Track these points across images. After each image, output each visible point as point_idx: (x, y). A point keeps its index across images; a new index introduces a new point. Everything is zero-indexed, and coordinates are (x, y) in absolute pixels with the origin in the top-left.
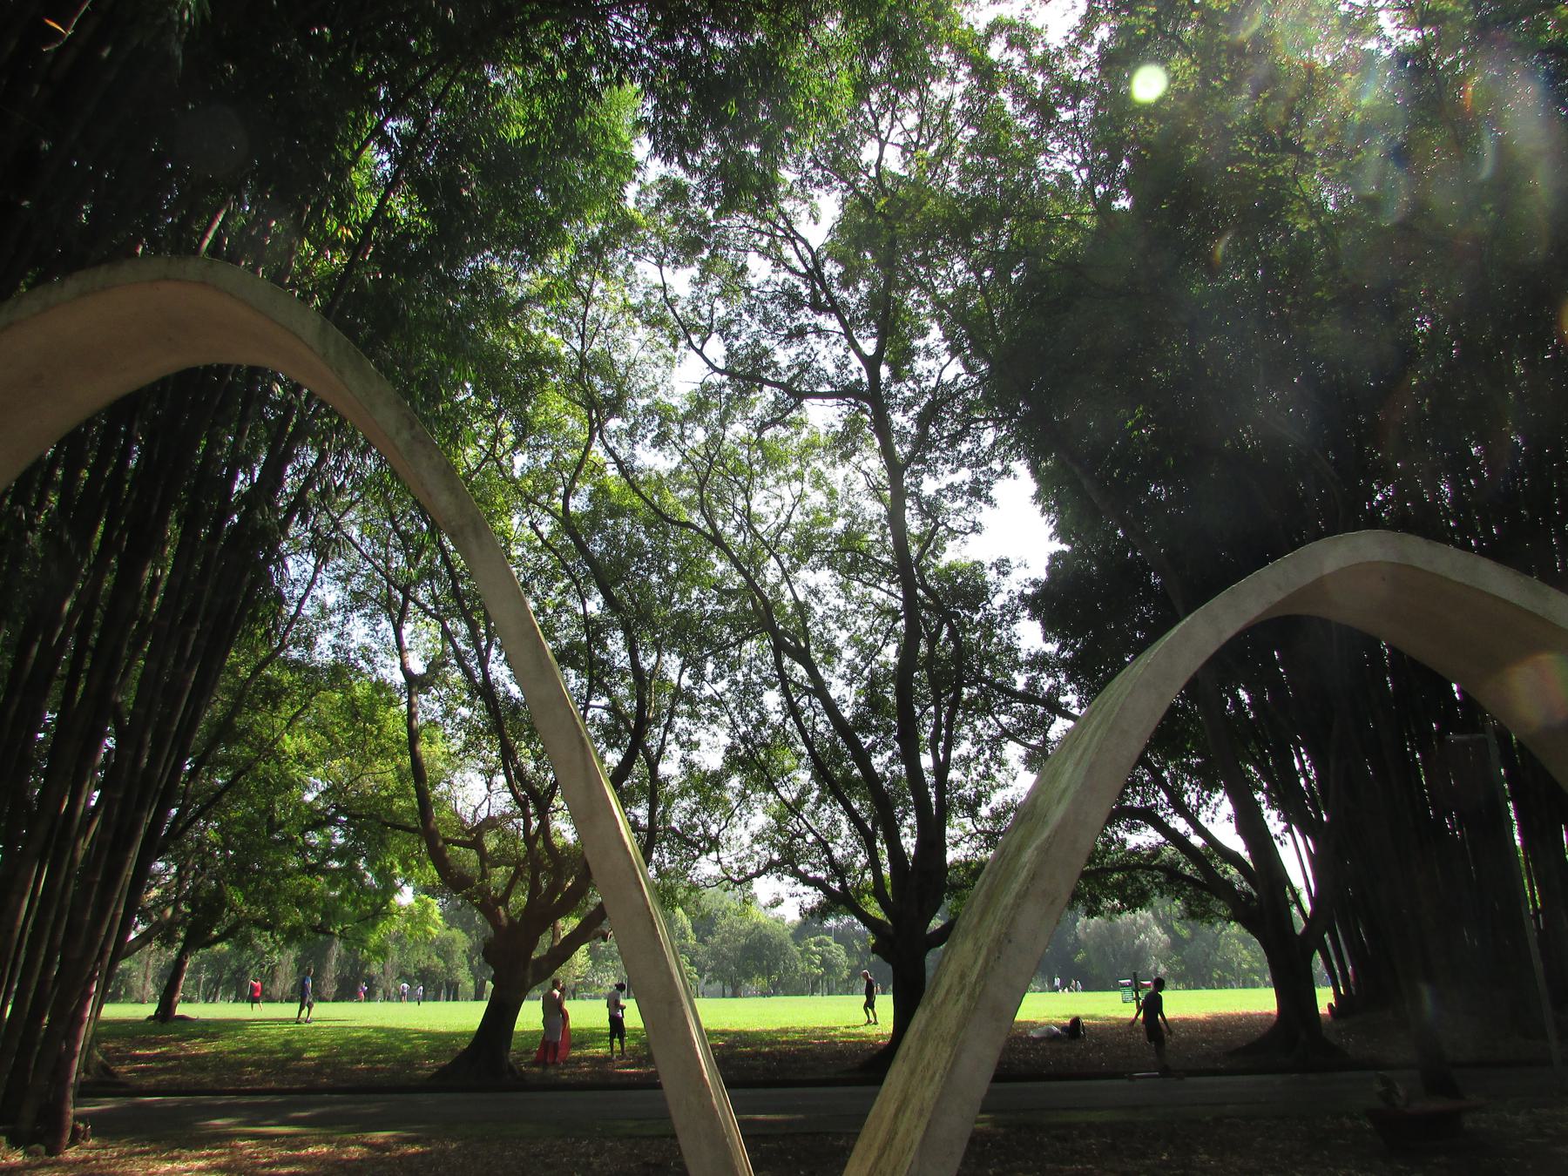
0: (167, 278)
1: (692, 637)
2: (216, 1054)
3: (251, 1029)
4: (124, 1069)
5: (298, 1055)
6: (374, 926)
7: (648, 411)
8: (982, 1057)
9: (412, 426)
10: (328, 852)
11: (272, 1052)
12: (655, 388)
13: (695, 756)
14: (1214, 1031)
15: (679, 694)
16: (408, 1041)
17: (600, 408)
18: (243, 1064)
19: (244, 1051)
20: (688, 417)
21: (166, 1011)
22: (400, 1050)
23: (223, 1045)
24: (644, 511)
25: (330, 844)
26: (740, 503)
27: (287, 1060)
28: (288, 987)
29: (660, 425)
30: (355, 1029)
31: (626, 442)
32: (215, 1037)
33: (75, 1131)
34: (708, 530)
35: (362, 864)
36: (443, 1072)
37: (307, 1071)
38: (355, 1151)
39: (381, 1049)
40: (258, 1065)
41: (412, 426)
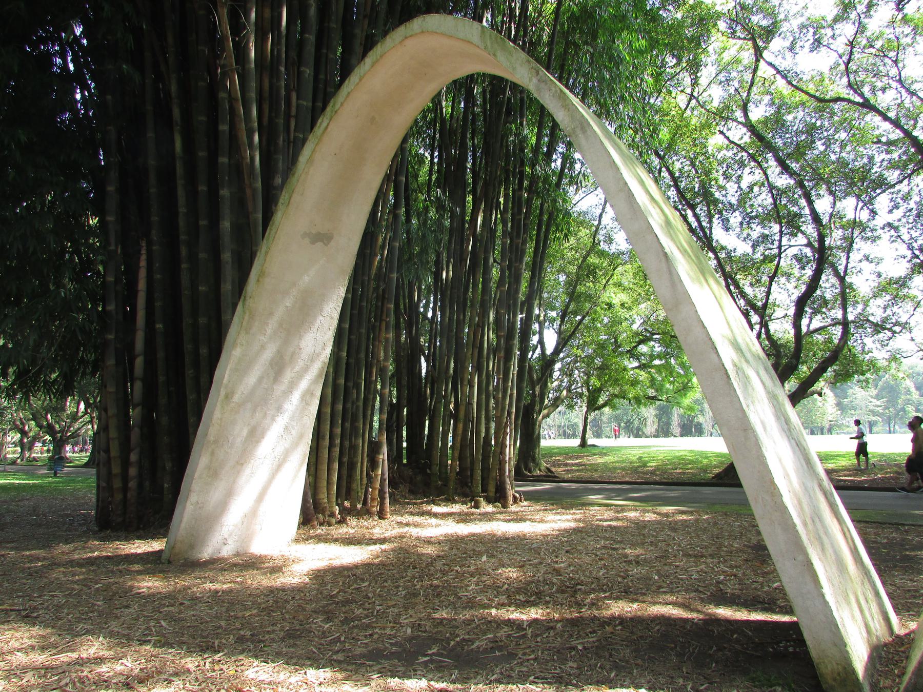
0: (406, 38)
1: (864, 184)
2: (603, 463)
3: (629, 451)
4: (560, 470)
5: (645, 465)
6: (685, 395)
7: (803, 27)
8: (169, 536)
9: (538, 73)
10: (652, 357)
11: (631, 463)
12: (806, 7)
13: (881, 268)
14: (126, 537)
15: (855, 224)
16: (706, 457)
17: (759, 38)
18: (615, 468)
19: (618, 462)
20: (836, 20)
21: (583, 444)
22: (701, 462)
23: (609, 459)
24: (812, 104)
25: (653, 351)
26: (893, 72)
27: (639, 467)
28: (653, 430)
29: (815, 34)
30: (679, 451)
31: (788, 55)
32: (605, 454)
33: (515, 498)
34: (858, 99)
35: (673, 361)
36: (718, 476)
37: (646, 473)
38: (650, 517)
39: (691, 462)
40: (623, 469)
41: (538, 73)
